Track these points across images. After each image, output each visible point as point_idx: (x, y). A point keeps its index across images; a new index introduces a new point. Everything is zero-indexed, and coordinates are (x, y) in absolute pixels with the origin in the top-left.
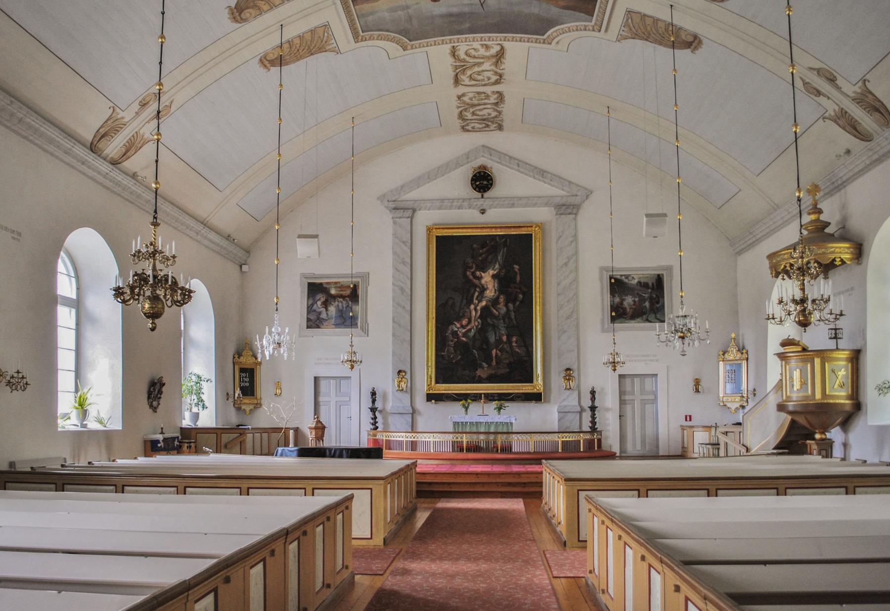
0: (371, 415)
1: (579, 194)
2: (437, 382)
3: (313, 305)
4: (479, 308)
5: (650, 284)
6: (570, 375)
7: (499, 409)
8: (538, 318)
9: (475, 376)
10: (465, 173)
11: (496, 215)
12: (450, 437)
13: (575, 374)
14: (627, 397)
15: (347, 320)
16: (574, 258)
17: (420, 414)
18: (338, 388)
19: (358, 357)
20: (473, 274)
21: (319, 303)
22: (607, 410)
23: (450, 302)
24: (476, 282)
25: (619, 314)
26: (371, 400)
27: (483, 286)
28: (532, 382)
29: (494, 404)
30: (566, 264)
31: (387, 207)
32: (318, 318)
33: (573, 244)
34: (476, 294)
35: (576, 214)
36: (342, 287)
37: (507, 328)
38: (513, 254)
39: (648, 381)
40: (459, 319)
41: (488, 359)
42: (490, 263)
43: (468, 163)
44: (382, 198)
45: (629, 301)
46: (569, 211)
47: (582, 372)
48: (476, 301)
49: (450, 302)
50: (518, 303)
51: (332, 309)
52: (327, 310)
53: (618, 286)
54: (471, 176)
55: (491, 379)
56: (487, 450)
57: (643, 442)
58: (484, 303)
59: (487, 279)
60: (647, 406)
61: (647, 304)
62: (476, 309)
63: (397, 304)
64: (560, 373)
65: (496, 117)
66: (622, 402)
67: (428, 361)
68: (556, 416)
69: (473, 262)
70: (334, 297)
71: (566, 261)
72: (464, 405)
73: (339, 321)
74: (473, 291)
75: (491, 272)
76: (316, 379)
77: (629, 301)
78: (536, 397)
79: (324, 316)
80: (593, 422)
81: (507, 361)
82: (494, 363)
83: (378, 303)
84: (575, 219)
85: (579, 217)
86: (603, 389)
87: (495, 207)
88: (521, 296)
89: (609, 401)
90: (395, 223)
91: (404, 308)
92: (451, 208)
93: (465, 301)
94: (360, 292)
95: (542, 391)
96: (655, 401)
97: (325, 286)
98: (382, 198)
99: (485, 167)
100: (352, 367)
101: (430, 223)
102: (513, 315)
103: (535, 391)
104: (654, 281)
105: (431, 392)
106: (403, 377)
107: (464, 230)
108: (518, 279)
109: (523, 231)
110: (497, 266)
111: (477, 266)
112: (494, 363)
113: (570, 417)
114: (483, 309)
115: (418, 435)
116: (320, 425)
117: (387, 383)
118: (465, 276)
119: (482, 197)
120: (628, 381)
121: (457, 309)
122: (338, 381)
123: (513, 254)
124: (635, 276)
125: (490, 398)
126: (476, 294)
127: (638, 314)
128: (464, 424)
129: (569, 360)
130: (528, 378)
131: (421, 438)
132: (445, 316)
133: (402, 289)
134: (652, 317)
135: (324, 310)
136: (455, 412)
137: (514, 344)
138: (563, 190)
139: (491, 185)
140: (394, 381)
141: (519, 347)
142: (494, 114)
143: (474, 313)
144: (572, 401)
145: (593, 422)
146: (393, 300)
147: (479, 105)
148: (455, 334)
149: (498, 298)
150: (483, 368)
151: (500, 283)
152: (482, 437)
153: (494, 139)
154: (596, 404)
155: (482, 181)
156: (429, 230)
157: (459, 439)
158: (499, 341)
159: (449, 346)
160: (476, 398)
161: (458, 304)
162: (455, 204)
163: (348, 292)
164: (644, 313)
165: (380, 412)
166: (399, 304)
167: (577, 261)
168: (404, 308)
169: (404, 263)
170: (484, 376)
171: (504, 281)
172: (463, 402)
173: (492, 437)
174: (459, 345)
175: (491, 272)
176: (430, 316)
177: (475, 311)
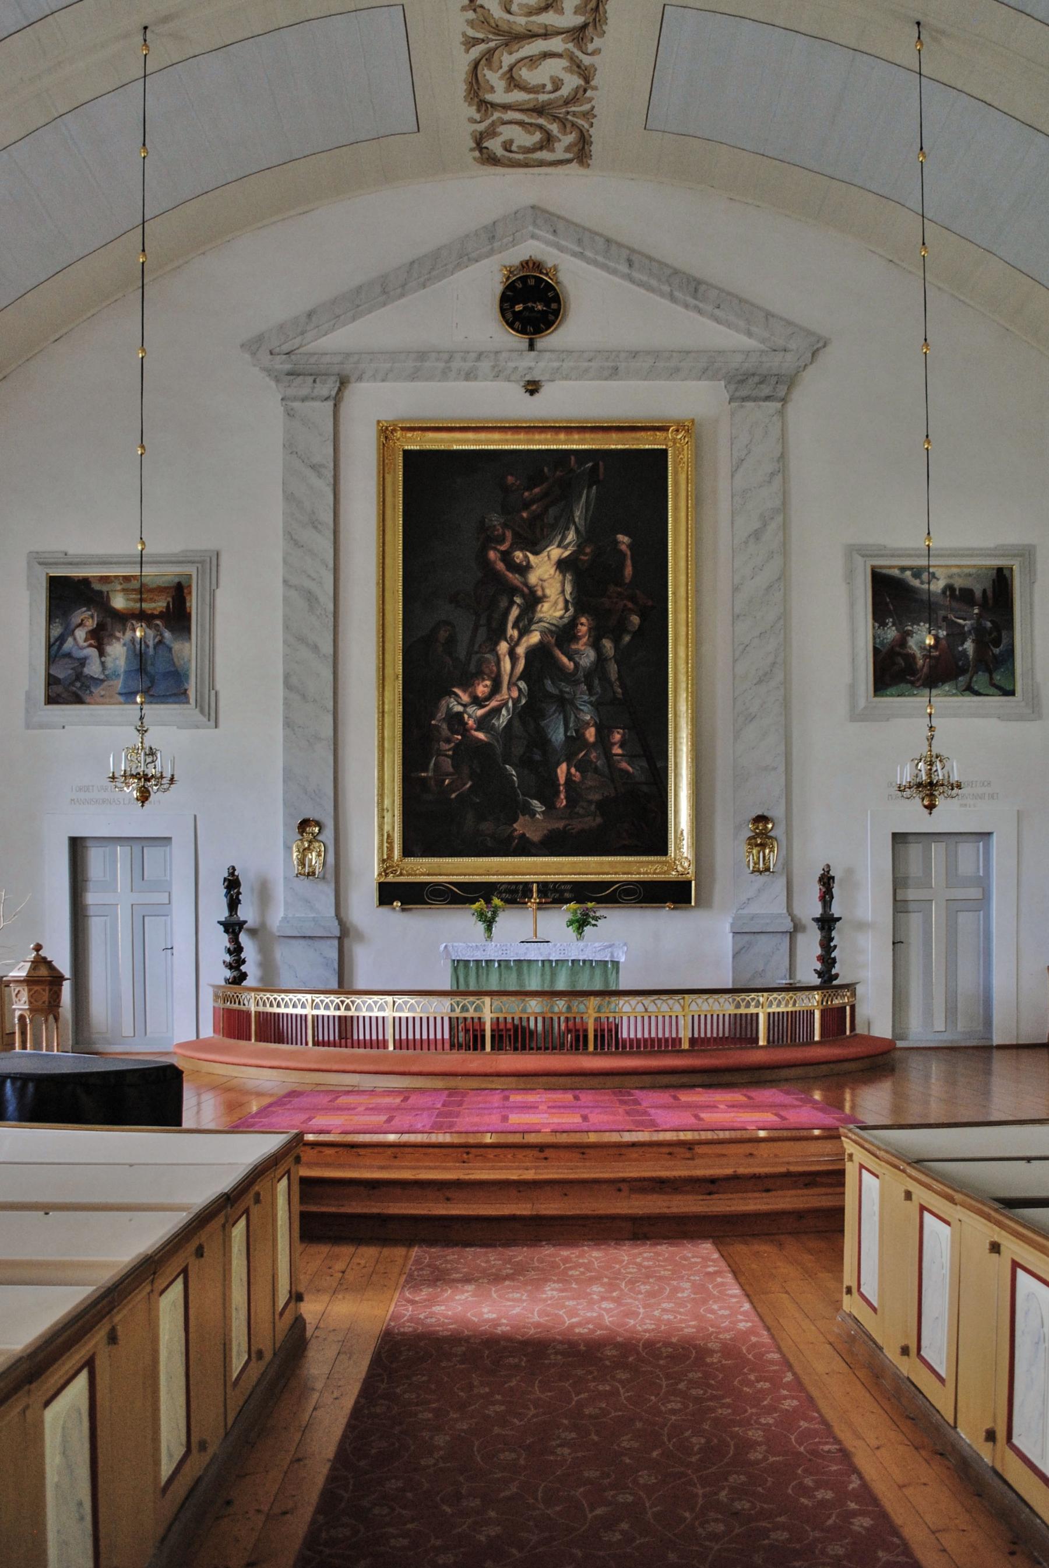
0: (224, 940)
1: (792, 345)
2: (407, 852)
3: (62, 639)
4: (521, 650)
5: (978, 594)
6: (765, 834)
7: (581, 923)
8: (682, 678)
9: (511, 837)
10: (484, 281)
11: (568, 395)
12: (441, 1008)
13: (779, 832)
14: (912, 894)
15: (160, 681)
16: (780, 519)
17: (360, 937)
18: (138, 870)
19: (161, 765)
20: (506, 557)
21: (80, 634)
22: (861, 926)
23: (443, 634)
24: (514, 578)
25: (893, 671)
26: (224, 902)
27: (532, 591)
28: (664, 852)
29: (569, 910)
30: (757, 535)
31: (268, 371)
32: (79, 676)
33: (778, 480)
34: (515, 612)
35: (784, 400)
36: (143, 590)
37: (597, 706)
38: (616, 499)
39: (966, 851)
40: (467, 682)
41: (547, 790)
42: (553, 527)
43: (491, 253)
44: (254, 345)
45: (924, 638)
46: (766, 390)
47: (796, 823)
48: (512, 632)
49: (443, 634)
50: (627, 638)
51: (118, 652)
52: (102, 653)
53: (892, 595)
54: (499, 289)
55: (555, 844)
56: (550, 1043)
57: (951, 1011)
58: (535, 638)
59: (545, 570)
60: (962, 917)
61: (969, 646)
62: (512, 653)
63: (295, 638)
64: (738, 828)
65: (573, 99)
66: (900, 907)
67: (381, 796)
68: (727, 943)
69: (505, 526)
70: (123, 619)
71: (757, 525)
72: (481, 915)
73: (136, 684)
74: (503, 604)
75: (555, 553)
76: (77, 846)
77: (924, 638)
78: (674, 894)
79: (93, 669)
80: (827, 960)
81: (596, 797)
82: (562, 801)
83: (242, 635)
84: (781, 413)
85: (790, 407)
86: (850, 871)
87: (567, 378)
88: (635, 619)
89: (866, 903)
90: (290, 414)
91: (315, 648)
92: (445, 375)
93: (482, 632)
94: (194, 604)
95: (691, 876)
96: (983, 903)
97: (97, 586)
98: (254, 345)
99: (538, 265)
100: (144, 796)
101: (388, 415)
102: (613, 669)
103: (673, 875)
104: (988, 585)
105: (391, 878)
106: (315, 838)
107: (483, 436)
108: (628, 571)
109: (646, 443)
110: (571, 536)
111: (516, 535)
112: (562, 801)
113: (764, 944)
114: (532, 653)
115: (358, 1000)
116: (43, 972)
117: (268, 853)
118: (486, 565)
119: (531, 347)
120: (914, 850)
121: (462, 652)
122: (137, 849)
123: (616, 499)
124: (939, 572)
125: (554, 894)
126: (515, 612)
127: (943, 672)
128: (483, 966)
129: (763, 796)
130: (654, 839)
131: (369, 1009)
132: (428, 672)
133: (311, 598)
134: (981, 680)
135: (93, 652)
136: (458, 932)
137: (617, 750)
138: (749, 334)
139: (557, 313)
140: (288, 848)
141: (631, 757)
142: (572, 82)
143: (507, 664)
144: (768, 904)
145: (827, 960)
146: (287, 627)
147: (531, 36)
148: (456, 720)
149: (573, 623)
150: (533, 814)
151: (577, 585)
152: (534, 1005)
153: (565, 189)
154: (836, 910)
155: (531, 304)
156: (386, 433)
157: (471, 1013)
158: (575, 741)
159: (440, 753)
160: (516, 894)
161: (464, 639)
162: (456, 365)
163: (158, 605)
164: (963, 671)
165: (253, 932)
166: (302, 640)
167: (785, 527)
168: (315, 648)
169: (315, 524)
170: (534, 835)
171: (586, 576)
172: (480, 904)
173: (561, 1004)
174: (469, 752)
175: (555, 553)
176: (389, 671)
177: (509, 658)
